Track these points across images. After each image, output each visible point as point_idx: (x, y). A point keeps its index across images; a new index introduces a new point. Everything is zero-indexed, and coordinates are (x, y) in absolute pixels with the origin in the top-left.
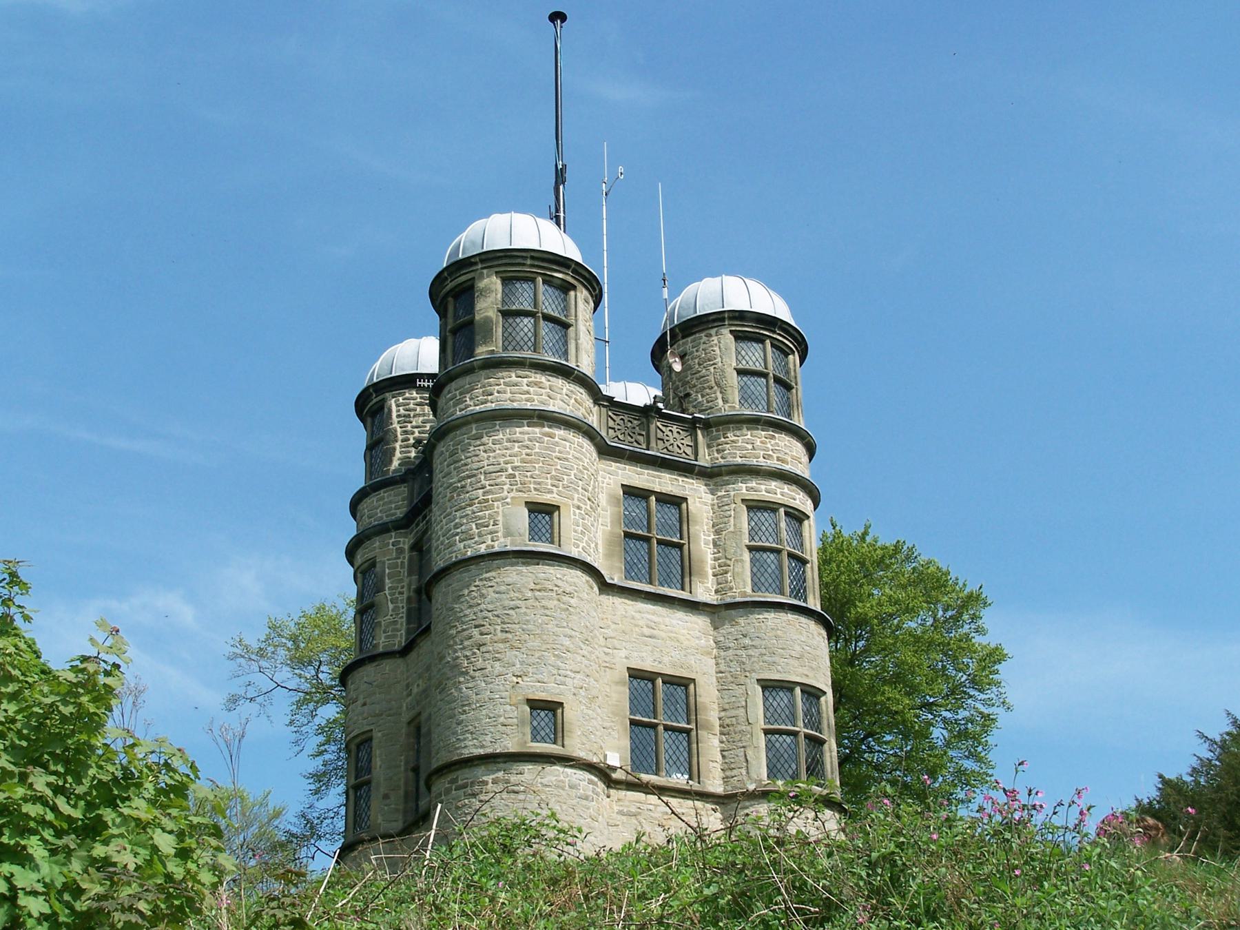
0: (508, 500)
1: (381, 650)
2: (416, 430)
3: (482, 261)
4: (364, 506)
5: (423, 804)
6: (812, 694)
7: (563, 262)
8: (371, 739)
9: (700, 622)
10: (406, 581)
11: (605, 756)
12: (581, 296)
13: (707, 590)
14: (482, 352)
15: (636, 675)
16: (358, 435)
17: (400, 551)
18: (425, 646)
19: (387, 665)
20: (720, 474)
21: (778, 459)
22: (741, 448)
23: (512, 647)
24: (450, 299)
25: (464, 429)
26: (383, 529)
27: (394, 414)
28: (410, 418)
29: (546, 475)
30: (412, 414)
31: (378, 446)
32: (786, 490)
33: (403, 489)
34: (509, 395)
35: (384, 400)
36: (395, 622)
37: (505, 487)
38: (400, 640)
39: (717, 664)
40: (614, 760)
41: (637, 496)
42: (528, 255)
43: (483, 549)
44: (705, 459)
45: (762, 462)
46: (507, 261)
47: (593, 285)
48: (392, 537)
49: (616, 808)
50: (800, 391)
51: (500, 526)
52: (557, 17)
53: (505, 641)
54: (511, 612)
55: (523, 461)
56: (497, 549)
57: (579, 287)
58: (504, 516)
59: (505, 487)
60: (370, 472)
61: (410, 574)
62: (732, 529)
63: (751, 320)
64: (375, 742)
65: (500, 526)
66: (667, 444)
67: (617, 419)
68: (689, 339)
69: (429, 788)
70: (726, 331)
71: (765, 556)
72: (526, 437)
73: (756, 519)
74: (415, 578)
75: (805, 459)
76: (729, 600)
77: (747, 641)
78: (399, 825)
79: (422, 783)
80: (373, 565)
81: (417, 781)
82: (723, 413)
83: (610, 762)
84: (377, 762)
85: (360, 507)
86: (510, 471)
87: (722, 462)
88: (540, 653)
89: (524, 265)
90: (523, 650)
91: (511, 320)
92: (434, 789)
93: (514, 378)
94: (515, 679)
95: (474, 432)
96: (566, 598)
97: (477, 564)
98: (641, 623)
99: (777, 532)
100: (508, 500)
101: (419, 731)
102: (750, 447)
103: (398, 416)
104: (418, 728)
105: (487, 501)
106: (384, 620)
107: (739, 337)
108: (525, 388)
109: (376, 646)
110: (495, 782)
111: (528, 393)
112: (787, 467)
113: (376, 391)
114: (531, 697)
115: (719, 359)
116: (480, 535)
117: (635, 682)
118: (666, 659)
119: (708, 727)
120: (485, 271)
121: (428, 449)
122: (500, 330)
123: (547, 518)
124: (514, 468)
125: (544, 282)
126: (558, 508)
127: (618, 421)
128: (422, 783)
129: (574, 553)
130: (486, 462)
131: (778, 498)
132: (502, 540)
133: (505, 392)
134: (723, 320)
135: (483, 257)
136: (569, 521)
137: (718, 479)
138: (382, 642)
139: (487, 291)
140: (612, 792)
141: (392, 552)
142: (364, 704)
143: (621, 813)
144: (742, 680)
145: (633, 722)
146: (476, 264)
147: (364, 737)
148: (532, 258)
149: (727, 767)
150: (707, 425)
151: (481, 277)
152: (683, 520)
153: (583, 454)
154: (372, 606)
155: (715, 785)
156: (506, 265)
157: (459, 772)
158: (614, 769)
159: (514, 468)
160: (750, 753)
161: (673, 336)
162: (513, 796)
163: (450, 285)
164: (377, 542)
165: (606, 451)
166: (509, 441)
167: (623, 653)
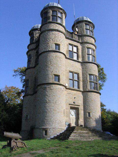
3: (49, 8)
5: (36, 90)
6: (96, 76)
8: (29, 80)
9: (79, 64)
11: (65, 84)
14: (48, 21)
17: (34, 53)
18: (37, 67)
19: (32, 69)
20: (83, 43)
24: (44, 14)
26: (32, 50)
28: (36, 34)
29: (60, 39)
31: (32, 39)
33: (35, 44)
35: (33, 32)
37: (51, 41)
38: (34, 66)
40: (67, 85)
42: (50, 7)
43: (47, 50)
44: (80, 41)
47: (65, 13)
49: (67, 93)
50: (94, 33)
53: (51, 65)
60: (30, 42)
64: (29, 81)
67: (68, 34)
69: (37, 88)
70: (84, 23)
75: (94, 42)
78: (32, 93)
79: (36, 87)
80: (30, 55)
81: (35, 86)
84: (29, 83)
92: (38, 88)
96: (60, 59)
101: (36, 79)
104: (36, 79)
106: (31, 63)
107: (86, 24)
110: (48, 88)
119: (81, 81)
121: (39, 37)
122: (51, 18)
126: (60, 45)
127: (68, 34)
128: (36, 87)
129: (62, 52)
131: (91, 47)
136: (61, 47)
138: (31, 66)
139: (49, 12)
140: (66, 90)
141: (33, 53)
143: (68, 93)
144: (86, 74)
149: (83, 87)
150: (81, 36)
151: (49, 10)
154: (30, 61)
156: (53, 9)
157: (42, 86)
158: (67, 86)
161: (76, 24)
162: (51, 90)
165: (66, 38)
166: (52, 34)
167: (69, 68)
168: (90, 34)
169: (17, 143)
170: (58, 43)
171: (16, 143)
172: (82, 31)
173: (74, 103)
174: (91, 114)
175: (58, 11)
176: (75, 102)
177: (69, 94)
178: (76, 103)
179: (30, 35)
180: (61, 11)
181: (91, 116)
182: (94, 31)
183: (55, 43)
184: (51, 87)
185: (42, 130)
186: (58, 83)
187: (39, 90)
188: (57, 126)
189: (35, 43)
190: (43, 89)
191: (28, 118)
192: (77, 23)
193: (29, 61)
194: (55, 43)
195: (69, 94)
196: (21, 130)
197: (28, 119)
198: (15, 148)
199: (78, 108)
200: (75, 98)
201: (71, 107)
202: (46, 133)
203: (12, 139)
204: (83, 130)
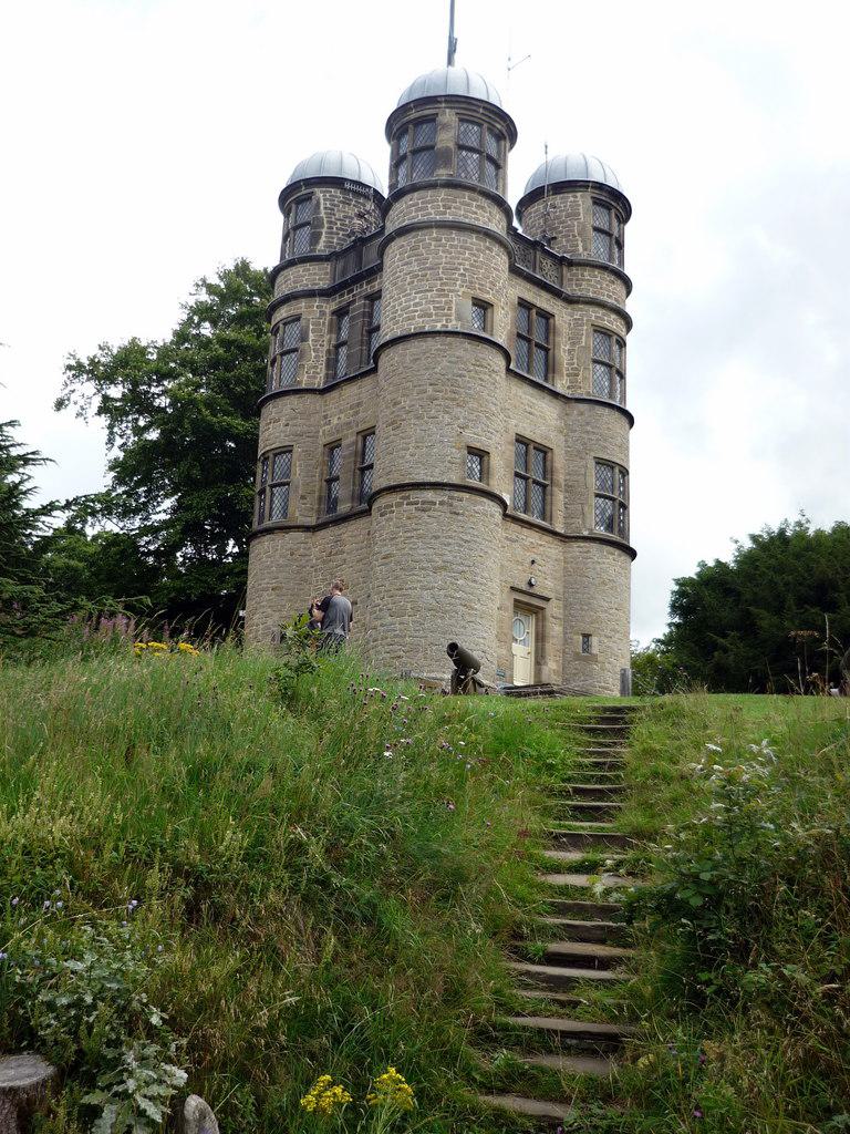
2: (339, 223)
3: (446, 101)
10: (326, 338)
15: (521, 440)
17: (323, 313)
19: (309, 398)
20: (577, 302)
23: (458, 405)
27: (322, 207)
30: (336, 209)
33: (328, 266)
42: (454, 99)
43: (439, 327)
45: (605, 299)
48: (317, 302)
51: (453, 311)
53: (454, 399)
56: (450, 329)
58: (457, 304)
61: (330, 332)
65: (453, 311)
74: (334, 336)
77: (589, 428)
82: (582, 257)
88: (476, 413)
99: (610, 352)
103: (326, 208)
106: (307, 364)
107: (596, 202)
109: (300, 383)
111: (476, 213)
119: (559, 486)
120: (447, 110)
125: (489, 129)
132: (454, 322)
137: (575, 306)
146: (440, 102)
150: (571, 264)
152: (549, 330)
157: (411, 492)
160: (586, 509)
164: (303, 303)
166: (461, 247)
167: (514, 422)
168: (481, 179)
173: (531, 585)
174: (594, 640)
175: (486, 125)
177: (513, 541)
181: (595, 650)
184: (455, 503)
186: (481, 485)
189: (327, 259)
195: (513, 541)
199: (543, 609)
200: (533, 562)
201: (516, 600)
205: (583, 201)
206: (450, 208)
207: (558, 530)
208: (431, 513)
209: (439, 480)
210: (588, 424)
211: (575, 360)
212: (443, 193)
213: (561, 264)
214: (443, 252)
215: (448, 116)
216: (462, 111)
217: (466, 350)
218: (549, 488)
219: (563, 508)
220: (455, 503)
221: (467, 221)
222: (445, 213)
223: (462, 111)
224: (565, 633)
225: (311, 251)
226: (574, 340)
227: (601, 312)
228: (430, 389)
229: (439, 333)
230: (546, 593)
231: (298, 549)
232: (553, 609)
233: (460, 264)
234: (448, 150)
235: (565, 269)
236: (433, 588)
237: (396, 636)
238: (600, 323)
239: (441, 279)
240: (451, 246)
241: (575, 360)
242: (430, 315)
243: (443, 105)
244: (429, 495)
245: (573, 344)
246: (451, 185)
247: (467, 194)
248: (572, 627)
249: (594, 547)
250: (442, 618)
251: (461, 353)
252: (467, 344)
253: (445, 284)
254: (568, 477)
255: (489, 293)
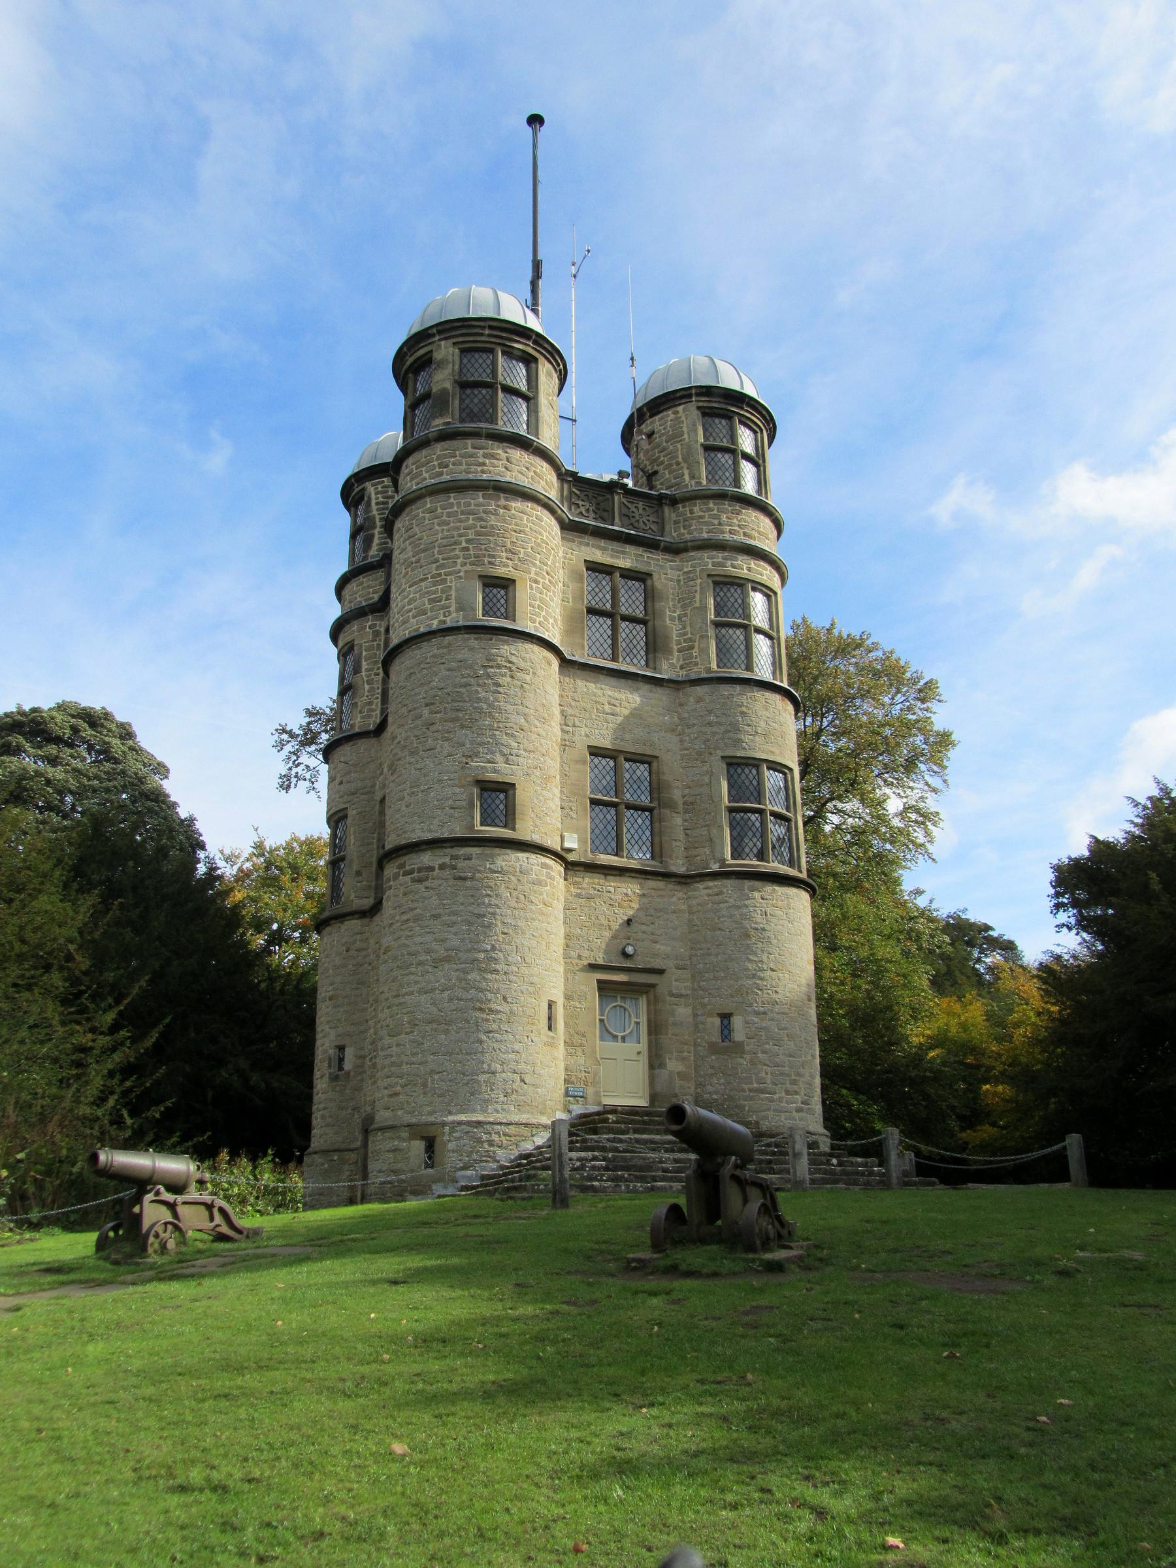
0: (462, 574)
1: (357, 730)
3: (439, 332)
4: (346, 592)
7: (524, 332)
8: (346, 816)
11: (562, 838)
12: (545, 369)
13: (673, 666)
16: (343, 521)
19: (363, 745)
21: (745, 534)
22: (707, 524)
23: (463, 727)
25: (419, 503)
27: (373, 502)
32: (753, 566)
34: (464, 467)
35: (364, 489)
36: (370, 703)
37: (459, 561)
39: (681, 741)
41: (601, 572)
43: (435, 624)
46: (471, 339)
47: (555, 355)
48: (370, 620)
51: (453, 600)
52: (535, 120)
54: (463, 690)
55: (478, 534)
56: (449, 624)
57: (542, 360)
58: (457, 591)
59: (459, 561)
62: (697, 605)
63: (719, 396)
66: (633, 520)
68: (657, 418)
71: (731, 631)
72: (481, 509)
73: (722, 594)
76: (694, 676)
83: (567, 845)
84: (352, 839)
85: (343, 593)
86: (464, 544)
87: (688, 537)
89: (482, 335)
90: (474, 729)
91: (468, 391)
93: (470, 450)
94: (465, 760)
95: (429, 506)
97: (429, 640)
98: (602, 700)
100: (462, 574)
102: (716, 522)
103: (377, 504)
105: (440, 575)
106: (361, 701)
107: (707, 413)
108: (481, 460)
109: (352, 726)
112: (752, 542)
113: (357, 481)
114: (480, 778)
115: (686, 436)
116: (432, 610)
117: (596, 761)
118: (628, 737)
120: (443, 343)
122: (457, 402)
123: (502, 592)
124: (468, 541)
125: (504, 353)
126: (514, 581)
130: (440, 535)
132: (454, 615)
133: (461, 464)
134: (690, 396)
135: (440, 328)
136: (524, 595)
137: (684, 555)
142: (341, 783)
145: (594, 802)
146: (433, 335)
147: (340, 814)
148: (491, 327)
150: (674, 501)
152: (650, 596)
153: (542, 527)
155: (678, 865)
157: (406, 858)
158: (570, 850)
159: (468, 541)
162: (459, 883)
163: (410, 360)
164: (355, 627)
166: (463, 513)
169: (181, 1209)
170: (503, 570)
171: (172, 1206)
172: (678, 464)
174: (737, 1022)
176: (630, 950)
178: (638, 958)
179: (348, 510)
180: (520, 346)
181: (739, 1035)
182: (774, 457)
183: (481, 577)
184: (461, 864)
185: (405, 1135)
187: (390, 888)
188: (502, 1112)
190: (413, 880)
191: (348, 1066)
192: (649, 409)
193: (346, 689)
194: (481, 577)
196: (308, 1146)
197: (348, 1073)
198: (161, 1232)
199: (653, 986)
201: (599, 981)
202: (430, 1158)
203: (149, 1188)
204: (651, 1133)
205: (687, 416)
206: (447, 466)
207: (674, 869)
208: (427, 884)
209: (437, 835)
210: (710, 712)
211: (688, 629)
212: (438, 449)
213: (661, 505)
214: (439, 525)
215: (445, 350)
216: (460, 339)
217: (472, 649)
218: (656, 812)
219: (682, 836)
220: (461, 864)
221: (471, 476)
222: (441, 474)
223: (460, 339)
224: (695, 1015)
225: (364, 558)
226: (685, 602)
227: (720, 556)
228: (426, 712)
229: (431, 634)
230: (657, 964)
231: (354, 942)
232: (676, 982)
233: (461, 536)
234: (444, 392)
235: (666, 509)
236: (433, 990)
237: (393, 1064)
238: (720, 570)
239: (437, 561)
240: (449, 515)
241: (688, 629)
242: (424, 613)
243: (437, 338)
244: (426, 858)
245: (684, 607)
246: (445, 436)
247: (469, 442)
248: (704, 1006)
249: (729, 884)
250: (447, 1032)
251: (464, 654)
252: (473, 641)
253: (442, 566)
254: (687, 791)
255: (506, 566)
